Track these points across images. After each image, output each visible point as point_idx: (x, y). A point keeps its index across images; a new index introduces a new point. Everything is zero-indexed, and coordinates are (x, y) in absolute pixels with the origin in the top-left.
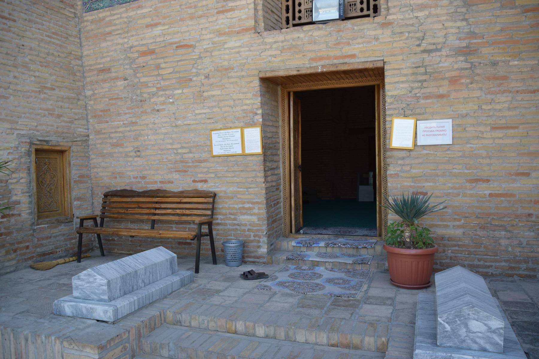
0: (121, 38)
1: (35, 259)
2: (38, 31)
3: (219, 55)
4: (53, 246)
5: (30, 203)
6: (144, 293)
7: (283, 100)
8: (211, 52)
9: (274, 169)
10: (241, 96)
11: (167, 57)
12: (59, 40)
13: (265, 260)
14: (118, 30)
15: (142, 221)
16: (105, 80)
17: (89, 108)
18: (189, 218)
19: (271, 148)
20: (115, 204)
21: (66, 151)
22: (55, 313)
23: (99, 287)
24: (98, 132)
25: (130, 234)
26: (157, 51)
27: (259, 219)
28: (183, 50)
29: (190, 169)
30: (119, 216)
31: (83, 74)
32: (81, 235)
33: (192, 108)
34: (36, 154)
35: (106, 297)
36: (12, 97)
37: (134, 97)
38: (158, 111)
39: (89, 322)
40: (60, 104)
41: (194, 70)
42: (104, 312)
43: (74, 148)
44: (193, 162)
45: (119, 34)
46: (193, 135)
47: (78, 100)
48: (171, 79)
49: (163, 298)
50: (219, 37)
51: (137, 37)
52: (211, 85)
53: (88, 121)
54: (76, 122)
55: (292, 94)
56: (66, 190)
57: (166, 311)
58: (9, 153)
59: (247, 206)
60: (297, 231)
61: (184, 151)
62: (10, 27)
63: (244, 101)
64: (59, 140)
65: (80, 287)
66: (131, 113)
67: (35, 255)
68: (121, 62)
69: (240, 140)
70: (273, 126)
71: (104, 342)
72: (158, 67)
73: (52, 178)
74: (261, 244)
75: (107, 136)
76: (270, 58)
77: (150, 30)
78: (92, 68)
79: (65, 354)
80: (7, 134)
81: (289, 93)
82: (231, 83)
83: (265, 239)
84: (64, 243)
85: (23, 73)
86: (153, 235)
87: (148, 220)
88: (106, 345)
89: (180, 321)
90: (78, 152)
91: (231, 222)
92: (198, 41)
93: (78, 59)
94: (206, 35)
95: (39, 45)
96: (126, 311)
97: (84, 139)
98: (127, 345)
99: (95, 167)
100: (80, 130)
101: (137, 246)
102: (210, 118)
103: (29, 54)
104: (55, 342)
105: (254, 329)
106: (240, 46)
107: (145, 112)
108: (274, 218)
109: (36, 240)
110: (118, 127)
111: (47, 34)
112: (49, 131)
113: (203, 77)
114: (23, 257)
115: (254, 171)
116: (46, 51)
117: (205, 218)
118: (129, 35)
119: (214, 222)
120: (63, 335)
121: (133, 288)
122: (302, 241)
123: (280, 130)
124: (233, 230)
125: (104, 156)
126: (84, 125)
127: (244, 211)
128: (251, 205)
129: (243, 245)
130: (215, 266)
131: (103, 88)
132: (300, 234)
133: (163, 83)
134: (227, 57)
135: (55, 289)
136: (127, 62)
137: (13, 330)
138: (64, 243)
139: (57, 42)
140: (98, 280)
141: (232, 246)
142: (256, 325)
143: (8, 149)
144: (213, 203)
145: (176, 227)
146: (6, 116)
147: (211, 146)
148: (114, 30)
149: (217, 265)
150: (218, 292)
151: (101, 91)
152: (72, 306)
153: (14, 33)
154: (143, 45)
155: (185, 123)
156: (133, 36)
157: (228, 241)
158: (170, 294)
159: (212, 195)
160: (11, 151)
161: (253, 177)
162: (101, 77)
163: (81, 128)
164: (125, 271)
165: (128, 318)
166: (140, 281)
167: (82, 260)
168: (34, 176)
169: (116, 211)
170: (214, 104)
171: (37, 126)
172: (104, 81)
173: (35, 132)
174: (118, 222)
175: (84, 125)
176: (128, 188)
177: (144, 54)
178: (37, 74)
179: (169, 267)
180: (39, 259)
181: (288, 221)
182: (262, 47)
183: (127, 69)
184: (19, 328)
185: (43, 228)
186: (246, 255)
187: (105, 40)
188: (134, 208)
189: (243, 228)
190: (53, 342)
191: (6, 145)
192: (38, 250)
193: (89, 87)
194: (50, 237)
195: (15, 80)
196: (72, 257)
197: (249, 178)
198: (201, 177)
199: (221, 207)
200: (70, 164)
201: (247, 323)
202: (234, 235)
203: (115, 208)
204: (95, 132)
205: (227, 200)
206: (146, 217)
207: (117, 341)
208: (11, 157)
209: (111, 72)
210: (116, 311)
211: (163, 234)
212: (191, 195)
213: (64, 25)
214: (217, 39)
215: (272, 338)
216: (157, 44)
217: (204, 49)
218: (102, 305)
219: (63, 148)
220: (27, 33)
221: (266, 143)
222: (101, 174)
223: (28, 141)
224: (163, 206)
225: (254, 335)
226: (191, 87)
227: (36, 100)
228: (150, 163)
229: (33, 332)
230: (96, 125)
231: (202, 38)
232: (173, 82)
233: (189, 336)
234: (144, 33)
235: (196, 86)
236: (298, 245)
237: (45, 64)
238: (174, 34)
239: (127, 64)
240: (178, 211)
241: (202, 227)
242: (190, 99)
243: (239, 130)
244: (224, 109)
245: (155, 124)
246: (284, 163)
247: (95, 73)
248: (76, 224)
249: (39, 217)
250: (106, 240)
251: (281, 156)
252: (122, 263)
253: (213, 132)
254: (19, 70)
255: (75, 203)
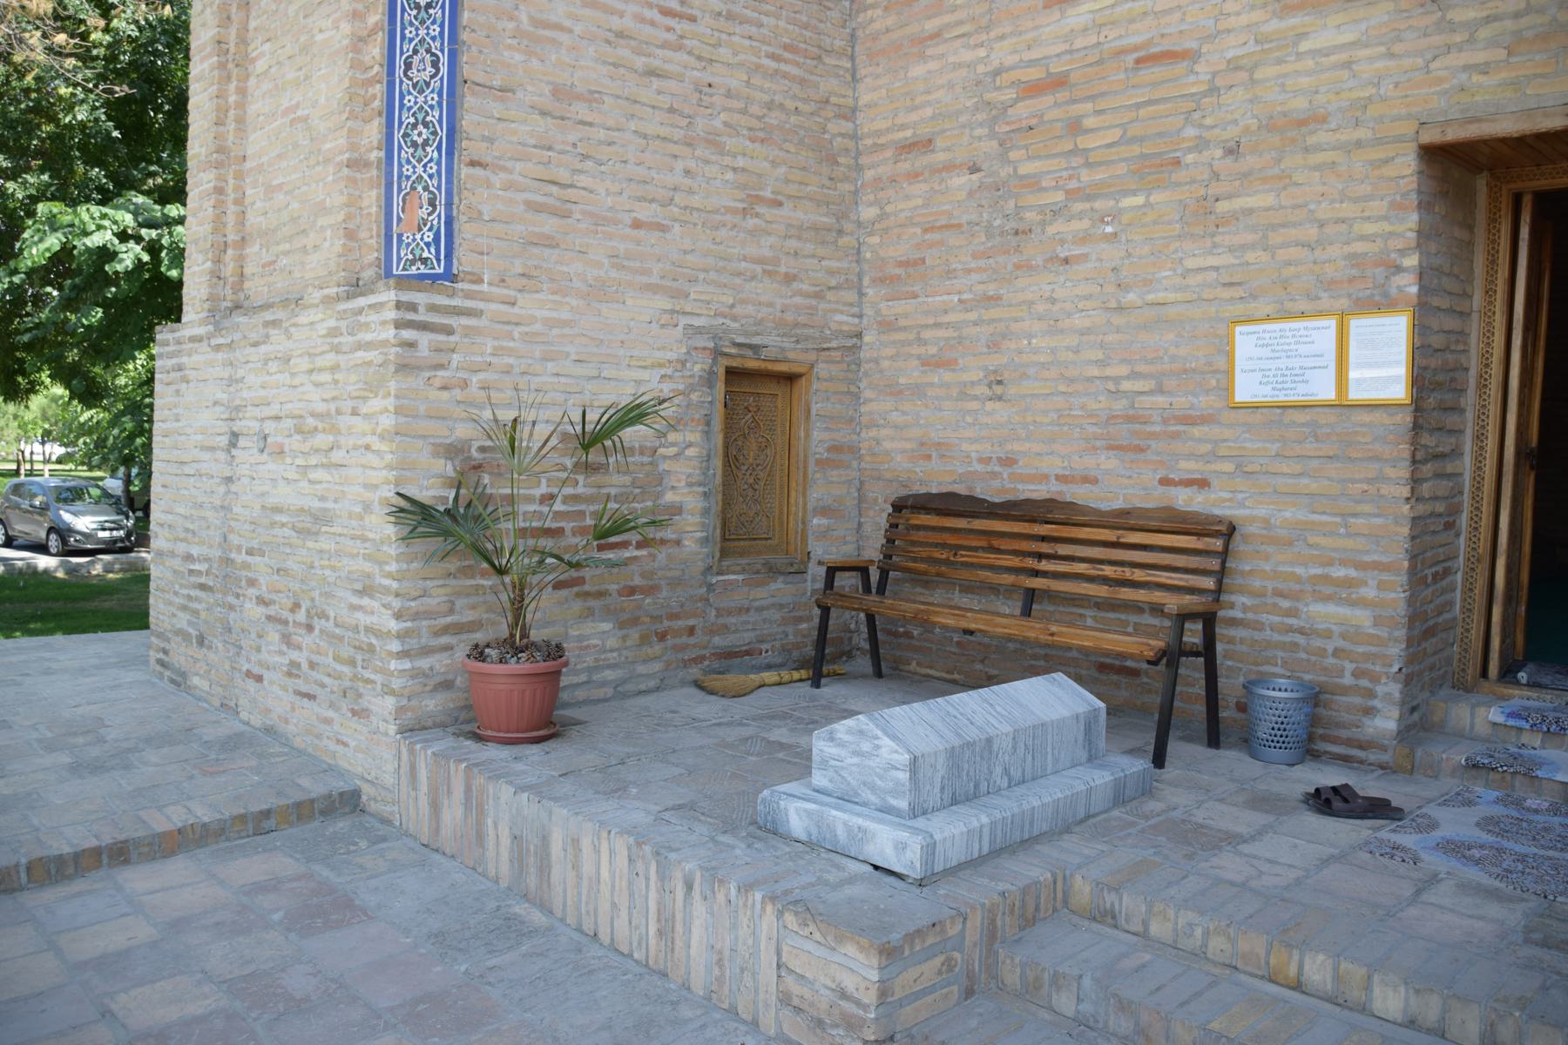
0: (967, 47)
1: (707, 663)
2: (747, 42)
3: (1279, 77)
4: (752, 634)
5: (706, 512)
6: (1009, 806)
7: (1493, 220)
8: (1251, 71)
9: (1443, 456)
10: (1347, 210)
11: (1103, 94)
12: (797, 64)
13: (1385, 757)
14: (960, 23)
15: (994, 589)
16: (917, 175)
17: (868, 255)
18: (1141, 595)
19: (1438, 386)
20: (921, 533)
21: (800, 376)
22: (761, 823)
23: (886, 770)
24: (887, 326)
25: (964, 624)
26: (1073, 78)
27: (1377, 621)
28: (1155, 70)
29: (1153, 444)
30: (933, 570)
31: (856, 159)
32: (825, 611)
33: (1176, 251)
34: (727, 382)
35: (903, 804)
36: (677, 228)
37: (997, 223)
38: (1066, 261)
39: (854, 867)
40: (793, 244)
41: (1191, 132)
42: (896, 848)
43: (822, 369)
44: (1165, 421)
45: (963, 35)
46: (1171, 336)
47: (840, 232)
48: (1112, 162)
49: (1061, 833)
50: (1281, 18)
51: (1014, 40)
52: (1246, 175)
53: (861, 294)
54: (830, 296)
55: (1527, 202)
56: (793, 484)
57: (1072, 875)
58: (662, 376)
59: (1339, 572)
60: (1508, 673)
61: (1139, 385)
62: (682, 37)
63: (1356, 227)
64: (786, 345)
65: (833, 763)
66: (985, 270)
67: (707, 652)
68: (963, 119)
69: (1331, 359)
70: (1451, 311)
71: (895, 937)
72: (1075, 127)
73: (761, 449)
74: (1376, 703)
75: (912, 337)
76: (1464, 77)
77: (1057, 15)
78: (882, 140)
79: (785, 949)
80: (663, 326)
81: (1517, 200)
82: (1317, 168)
83: (1395, 689)
84: (781, 629)
85: (707, 162)
86: (1032, 634)
87: (1014, 587)
88: (902, 947)
89: (1113, 912)
90: (830, 379)
91: (1277, 619)
92: (1210, 38)
93: (845, 117)
94: (1238, 14)
95: (748, 82)
96: (956, 855)
97: (850, 343)
98: (957, 955)
99: (873, 424)
100: (839, 317)
101: (981, 664)
102: (1231, 284)
103: (725, 109)
104: (763, 909)
105: (1368, 988)
106: (1353, 44)
107: (1026, 267)
108: (1431, 623)
109: (714, 613)
110: (946, 312)
111: (771, 49)
112: (762, 319)
113: (1219, 153)
114: (680, 656)
115: (1376, 458)
116: (766, 98)
117: (1195, 598)
118: (993, 34)
119: (1221, 614)
120: (786, 893)
121: (976, 786)
122: (1526, 709)
123: (1475, 325)
124: (1283, 646)
125: (901, 392)
126: (851, 305)
127: (1328, 590)
128: (1353, 573)
129: (1315, 698)
130: (1212, 752)
131: (908, 198)
132: (1517, 683)
133: (1086, 176)
134: (1304, 81)
135: (758, 755)
136: (981, 117)
137: (658, 854)
138: (781, 629)
139: (794, 71)
140: (884, 752)
141: (1279, 695)
142: (1376, 978)
143: (661, 365)
144: (1225, 554)
145: (1094, 618)
146: (662, 278)
147: (1230, 373)
148: (949, 26)
149: (1221, 752)
150: (1233, 840)
151: (901, 206)
152: (808, 813)
153: (690, 53)
154: (1032, 63)
155: (1150, 297)
156: (1002, 37)
157: (1263, 680)
158: (1081, 821)
159: (1223, 528)
160: (669, 372)
161: (1369, 481)
162: (904, 166)
163: (842, 312)
164: (959, 735)
165: (961, 874)
166: (998, 770)
167: (823, 681)
168: (719, 439)
169: (923, 552)
170: (1250, 238)
171: (732, 306)
172: (914, 176)
173: (728, 322)
174: (926, 584)
175: (851, 305)
176: (961, 489)
177: (1033, 90)
178: (740, 162)
179: (1081, 738)
180: (716, 665)
181: (1476, 634)
182: (1437, 40)
183: (980, 138)
184: (672, 850)
185: (731, 582)
186: (1321, 731)
187: (922, 57)
188: (975, 549)
189: (1318, 643)
190: (758, 906)
191: (659, 355)
192: (717, 640)
193: (871, 197)
194: (748, 610)
195: (688, 181)
196: (796, 669)
197: (1354, 481)
198: (1188, 471)
199: (1247, 568)
200: (809, 411)
201: (1344, 966)
202: (1285, 663)
203: (921, 544)
204: (879, 323)
205: (1270, 549)
206: (1008, 579)
207: (930, 941)
208: (666, 389)
209: (933, 151)
210: (930, 850)
211: (1060, 634)
212: (1154, 524)
213: (814, 22)
214: (1274, 25)
215: (1429, 1031)
216: (1076, 56)
217: (1229, 62)
218: (890, 823)
219: (796, 369)
220: (721, 50)
221: (1425, 368)
222: (887, 445)
223: (711, 345)
224: (1063, 550)
225: (1364, 1009)
226: (1179, 184)
227: (734, 233)
228: (1029, 419)
229: (707, 870)
230: (883, 305)
231: (1222, 25)
232: (1119, 172)
233: (1144, 966)
234: (1036, 28)
235: (1193, 181)
236: (1511, 722)
237: (761, 135)
238: (1132, 21)
239: (981, 125)
240: (1108, 571)
241: (1187, 625)
242: (1170, 223)
243: (1331, 323)
244: (1282, 254)
245: (1053, 301)
246: (1479, 437)
247: (889, 153)
248: (814, 581)
249: (724, 553)
250: (889, 633)
251: (1469, 415)
252: (951, 709)
253: (1239, 329)
254: (698, 152)
255: (815, 521)
